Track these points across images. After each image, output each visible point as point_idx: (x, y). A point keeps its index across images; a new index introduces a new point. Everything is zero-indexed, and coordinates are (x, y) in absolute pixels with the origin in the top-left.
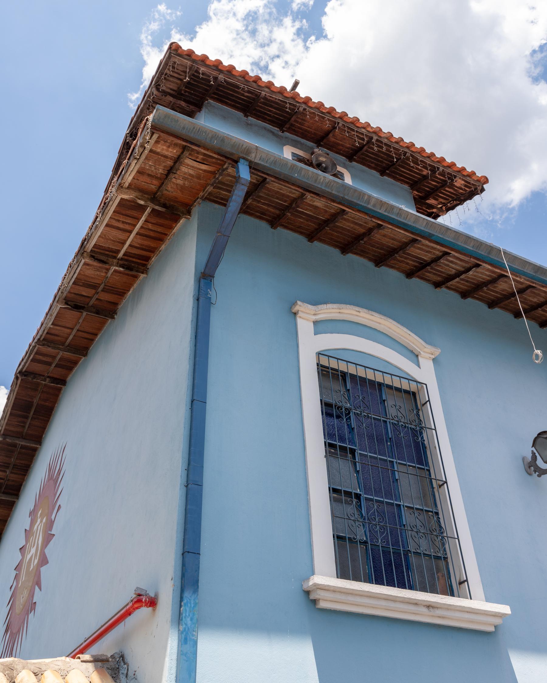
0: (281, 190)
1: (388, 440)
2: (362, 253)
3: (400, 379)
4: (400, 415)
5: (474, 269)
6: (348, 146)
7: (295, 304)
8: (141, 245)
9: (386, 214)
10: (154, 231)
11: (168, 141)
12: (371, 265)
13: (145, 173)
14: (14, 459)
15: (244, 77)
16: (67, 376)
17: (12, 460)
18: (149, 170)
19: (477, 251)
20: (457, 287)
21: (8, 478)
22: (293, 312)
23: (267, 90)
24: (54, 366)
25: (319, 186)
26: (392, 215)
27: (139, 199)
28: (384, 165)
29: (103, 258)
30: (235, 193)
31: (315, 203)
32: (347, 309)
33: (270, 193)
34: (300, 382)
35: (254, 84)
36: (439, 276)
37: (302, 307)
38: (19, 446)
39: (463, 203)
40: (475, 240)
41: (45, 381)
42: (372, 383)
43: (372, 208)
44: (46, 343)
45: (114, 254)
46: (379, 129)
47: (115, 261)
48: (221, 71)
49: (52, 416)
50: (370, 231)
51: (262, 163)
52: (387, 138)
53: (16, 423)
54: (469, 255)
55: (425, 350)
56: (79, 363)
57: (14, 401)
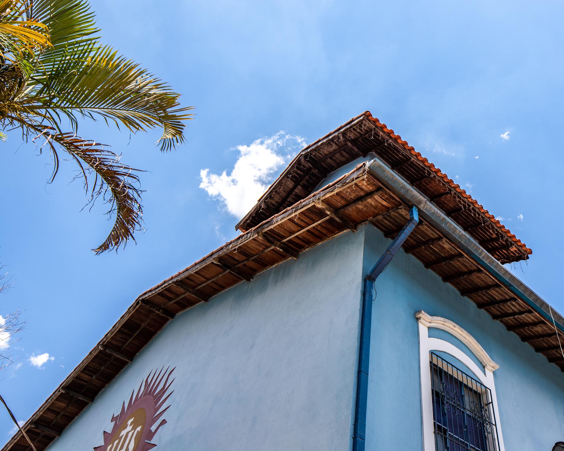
0: (426, 231)
1: (465, 427)
2: (456, 285)
3: (471, 380)
4: (476, 410)
5: (526, 313)
6: (451, 206)
7: (419, 312)
8: (304, 238)
9: (489, 265)
10: (320, 232)
11: (371, 181)
12: (458, 293)
13: (340, 195)
14: (104, 367)
15: (403, 145)
16: (178, 311)
17: (102, 368)
18: (345, 194)
19: (535, 303)
20: (507, 322)
21: (92, 382)
22: (416, 317)
23: (415, 157)
24: (174, 302)
25: (455, 236)
26: (492, 266)
27: (328, 210)
28: (469, 224)
29: (271, 239)
30: (407, 227)
31: (444, 245)
32: (448, 323)
33: (418, 231)
34: (420, 371)
35: (408, 151)
36: (499, 311)
37: (424, 316)
38: (113, 357)
39: (511, 262)
40: (535, 295)
41: (159, 312)
42: (456, 380)
43: (482, 259)
44: (180, 284)
45: (279, 238)
46: (475, 201)
47: (278, 243)
48: (391, 138)
49: (152, 340)
50: (470, 272)
51: (426, 212)
52: (478, 208)
53: (119, 339)
54: (528, 304)
55: (491, 364)
56: (196, 305)
57: (127, 321)
